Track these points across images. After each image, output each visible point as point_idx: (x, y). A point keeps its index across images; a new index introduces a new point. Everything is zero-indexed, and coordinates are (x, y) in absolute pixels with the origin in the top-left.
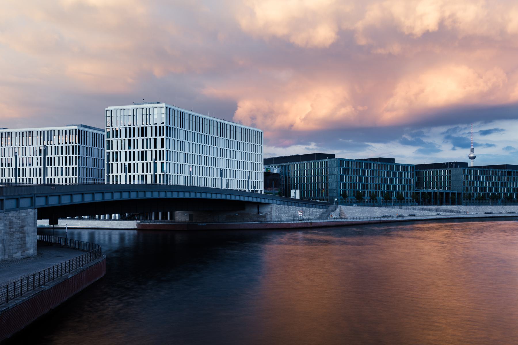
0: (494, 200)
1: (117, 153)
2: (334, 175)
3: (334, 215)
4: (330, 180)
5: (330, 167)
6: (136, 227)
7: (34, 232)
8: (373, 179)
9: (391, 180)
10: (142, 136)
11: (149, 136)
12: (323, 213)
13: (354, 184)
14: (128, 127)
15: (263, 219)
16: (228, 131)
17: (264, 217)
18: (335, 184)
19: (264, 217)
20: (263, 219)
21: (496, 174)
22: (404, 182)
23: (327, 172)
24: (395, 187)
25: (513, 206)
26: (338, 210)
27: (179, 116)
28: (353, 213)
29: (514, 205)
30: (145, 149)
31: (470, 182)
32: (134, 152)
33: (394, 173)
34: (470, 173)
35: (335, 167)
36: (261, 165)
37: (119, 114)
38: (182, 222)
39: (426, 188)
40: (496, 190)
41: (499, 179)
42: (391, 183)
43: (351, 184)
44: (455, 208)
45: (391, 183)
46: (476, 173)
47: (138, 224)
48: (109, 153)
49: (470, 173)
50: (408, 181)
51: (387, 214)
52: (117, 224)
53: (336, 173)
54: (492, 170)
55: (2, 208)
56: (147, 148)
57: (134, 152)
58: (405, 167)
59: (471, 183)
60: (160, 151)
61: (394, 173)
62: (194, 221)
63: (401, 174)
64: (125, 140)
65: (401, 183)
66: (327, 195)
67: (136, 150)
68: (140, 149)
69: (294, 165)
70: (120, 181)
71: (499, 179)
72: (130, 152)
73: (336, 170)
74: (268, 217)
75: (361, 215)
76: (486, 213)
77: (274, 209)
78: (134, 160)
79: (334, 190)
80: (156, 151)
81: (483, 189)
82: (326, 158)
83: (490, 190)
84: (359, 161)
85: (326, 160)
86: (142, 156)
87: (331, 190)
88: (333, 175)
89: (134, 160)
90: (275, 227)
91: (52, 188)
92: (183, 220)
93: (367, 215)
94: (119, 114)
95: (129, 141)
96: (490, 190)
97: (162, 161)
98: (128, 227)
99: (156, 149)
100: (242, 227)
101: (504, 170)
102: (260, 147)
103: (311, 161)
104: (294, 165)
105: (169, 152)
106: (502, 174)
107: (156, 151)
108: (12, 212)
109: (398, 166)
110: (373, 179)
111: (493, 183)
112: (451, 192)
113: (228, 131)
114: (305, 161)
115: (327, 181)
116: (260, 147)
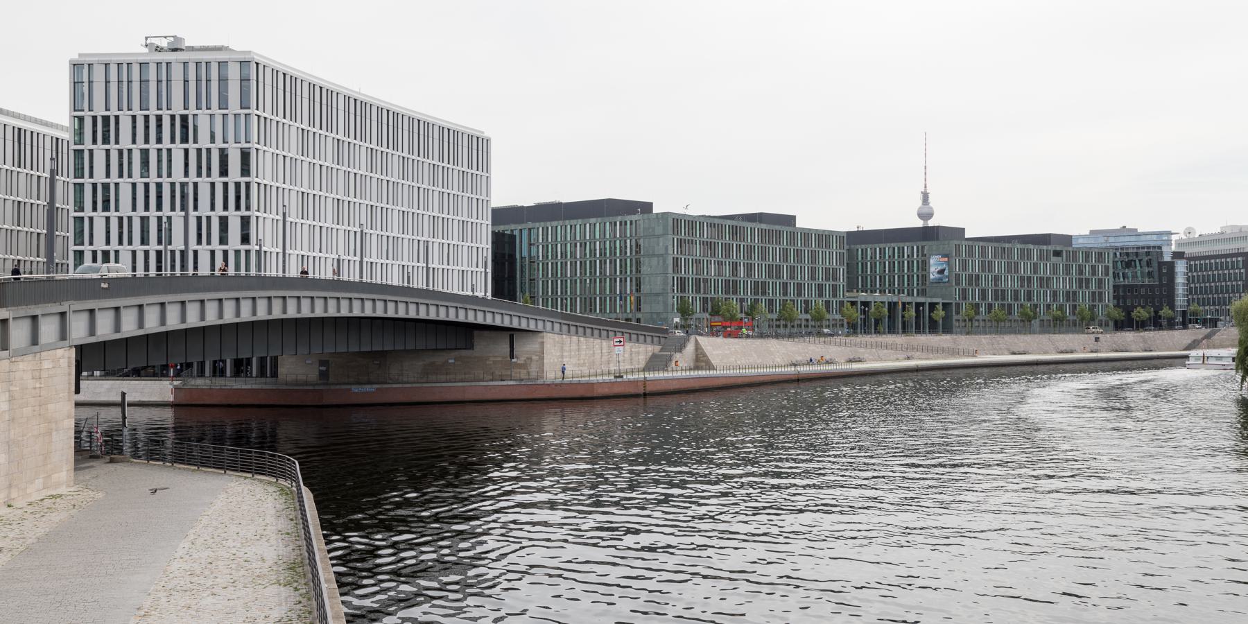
0: (1026, 322)
1: (106, 187)
2: (658, 256)
3: (685, 357)
4: (644, 269)
5: (645, 237)
6: (172, 399)
7: (69, 417)
8: (749, 268)
9: (792, 270)
10: (106, 140)
11: (126, 142)
12: (654, 356)
13: (1004, 291)
14: (140, 114)
15: (523, 374)
16: (406, 133)
17: (524, 366)
18: (659, 279)
19: (524, 366)
20: (523, 374)
21: (1029, 257)
22: (820, 274)
23: (638, 245)
24: (799, 287)
25: (1071, 336)
26: (690, 348)
27: (288, 89)
28: (732, 356)
29: (1073, 332)
30: (114, 178)
31: (970, 276)
32: (159, 186)
33: (798, 253)
34: (970, 252)
35: (658, 236)
36: (484, 227)
37: (192, 76)
38: (297, 383)
39: (882, 292)
40: (1029, 296)
41: (1035, 268)
42: (792, 277)
43: (996, 291)
44: (963, 341)
45: (792, 277)
46: (983, 252)
47: (176, 388)
48: (82, 185)
49: (970, 252)
50: (831, 274)
51: (799, 358)
52: (109, 390)
53: (662, 251)
54: (1019, 246)
55: (5, 348)
56: (121, 176)
57: (159, 186)
58: (824, 237)
59: (974, 280)
60: (238, 185)
61: (798, 253)
62: (331, 380)
63: (814, 255)
64: (130, 151)
65: (813, 278)
66: (639, 310)
67: (165, 181)
68: (178, 176)
69: (545, 230)
70: (196, 268)
71: (1035, 268)
72: (147, 185)
73: (668, 245)
74: (534, 369)
75: (743, 361)
76: (1014, 353)
77: (547, 346)
78: (159, 208)
79: (657, 295)
80: (226, 185)
81: (1000, 294)
82: (635, 213)
83: (1016, 295)
84: (716, 221)
85: (634, 218)
86: (185, 198)
87: (650, 294)
88: (654, 255)
89: (159, 208)
90: (555, 395)
91: (103, 285)
92: (302, 378)
93: (754, 359)
94: (192, 76)
95: (145, 154)
96: (1016, 295)
97: (244, 213)
98: (145, 399)
99: (225, 179)
100: (470, 396)
101: (1045, 247)
102: (484, 179)
103: (593, 220)
104: (545, 230)
105: (262, 187)
106: (1041, 257)
107: (226, 185)
108: (25, 358)
109: (807, 234)
110: (749, 268)
111: (1022, 279)
112: (929, 300)
113: (406, 133)
114: (577, 218)
115: (638, 271)
116: (484, 179)
